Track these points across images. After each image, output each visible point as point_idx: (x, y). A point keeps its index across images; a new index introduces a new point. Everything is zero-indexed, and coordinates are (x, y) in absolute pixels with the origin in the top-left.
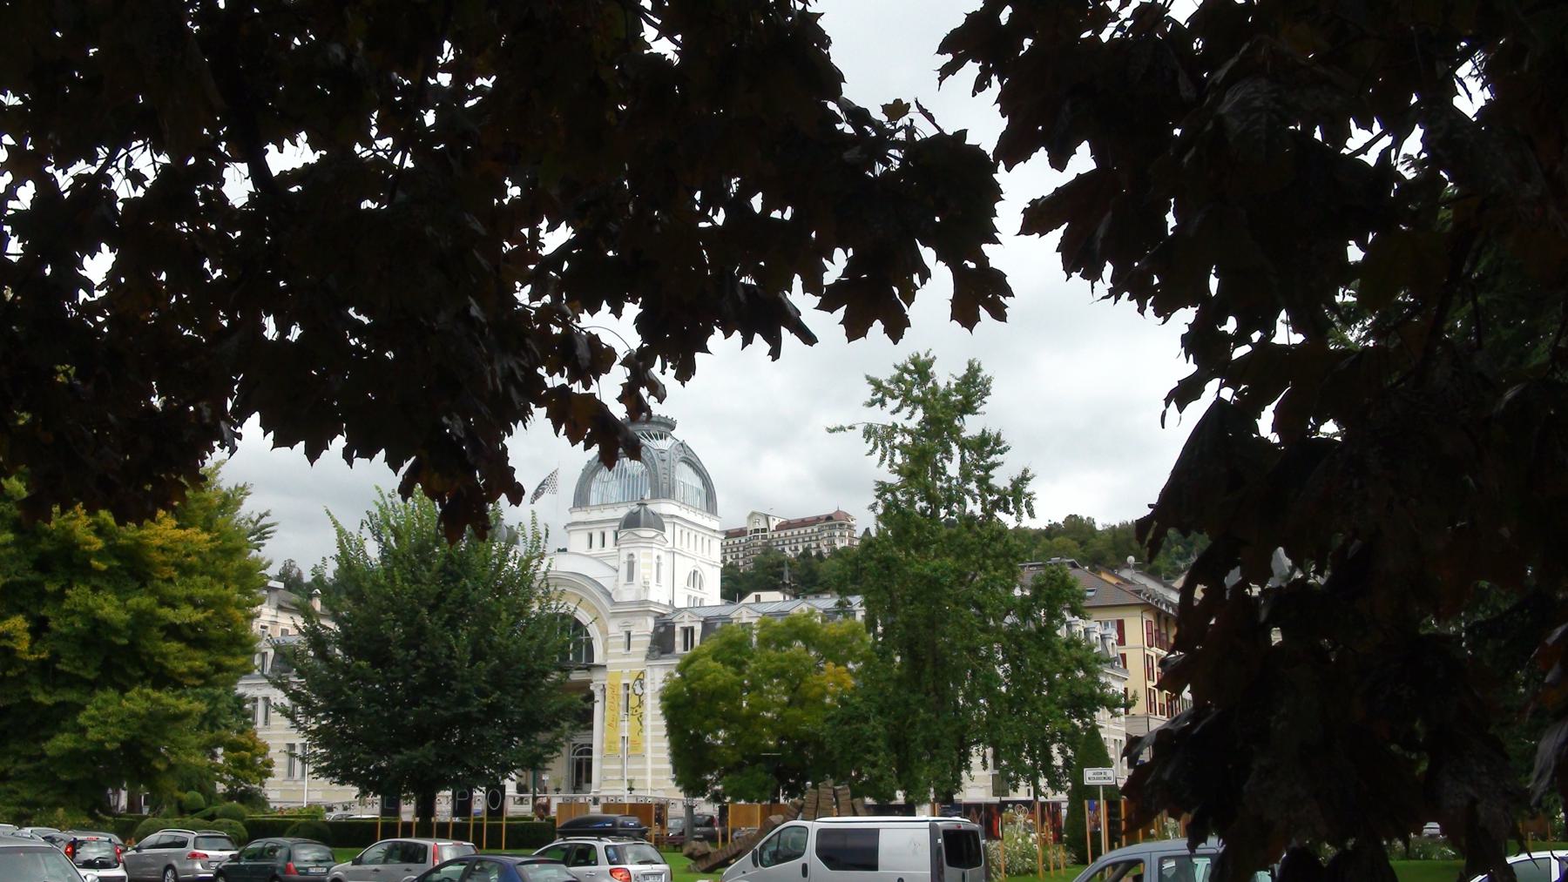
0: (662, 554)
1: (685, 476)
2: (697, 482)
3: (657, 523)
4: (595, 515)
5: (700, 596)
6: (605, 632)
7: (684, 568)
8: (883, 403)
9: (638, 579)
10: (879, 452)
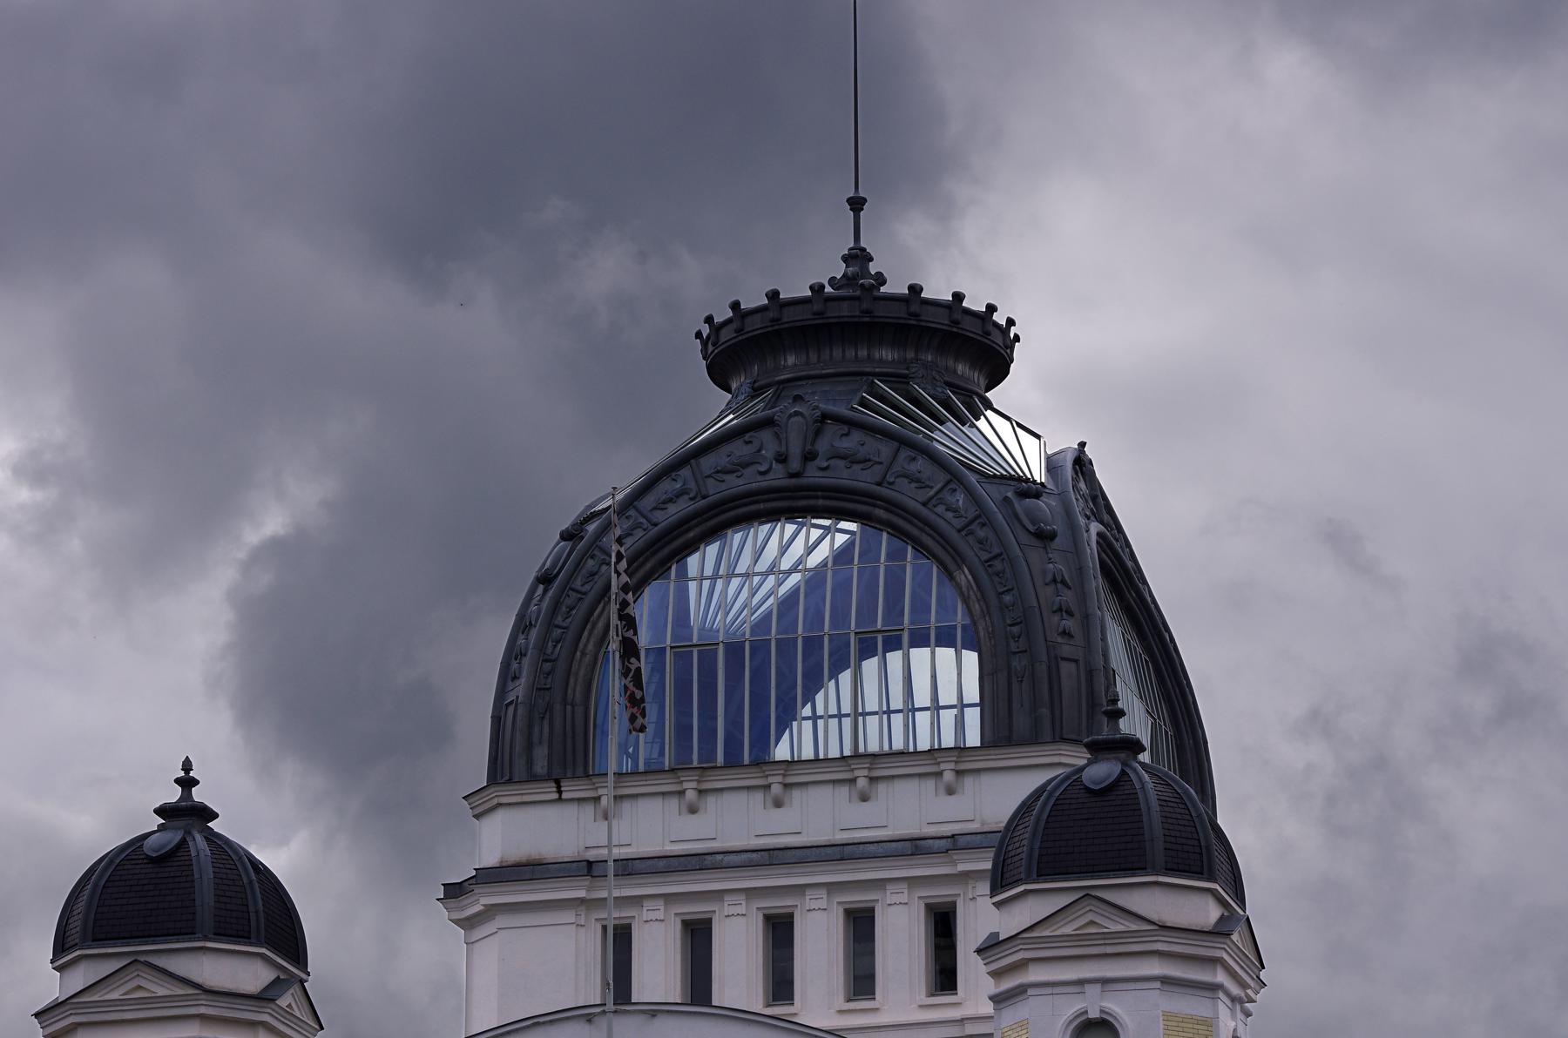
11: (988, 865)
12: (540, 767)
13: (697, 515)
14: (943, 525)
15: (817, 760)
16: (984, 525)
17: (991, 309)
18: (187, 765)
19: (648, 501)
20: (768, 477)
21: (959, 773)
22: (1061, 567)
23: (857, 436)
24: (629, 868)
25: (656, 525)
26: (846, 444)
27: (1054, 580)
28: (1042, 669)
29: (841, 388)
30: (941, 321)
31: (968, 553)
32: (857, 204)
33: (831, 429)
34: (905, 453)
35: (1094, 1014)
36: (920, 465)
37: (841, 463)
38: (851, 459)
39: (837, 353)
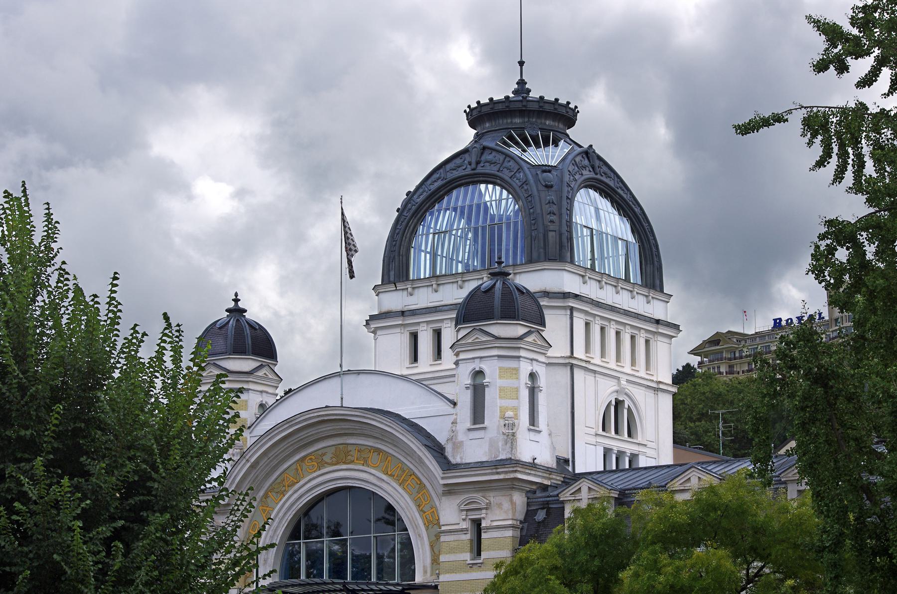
0: (540, 370)
1: (591, 212)
2: (616, 225)
3: (525, 309)
4: (423, 298)
5: (629, 448)
6: (433, 522)
7: (593, 396)
8: (842, 68)
9: (492, 418)
10: (834, 161)
11: (455, 316)
12: (392, 279)
13: (443, 186)
14: (514, 184)
15: (425, 278)
17: (568, 103)
18: (236, 295)
19: (429, 182)
21: (414, 288)
23: (494, 153)
24: (414, 313)
26: (490, 157)
28: (541, 236)
30: (535, 106)
31: (521, 195)
32: (521, 63)
33: (487, 152)
34: (508, 159)
35: (477, 369)
36: (512, 163)
37: (487, 164)
38: (491, 163)
39: (501, 121)
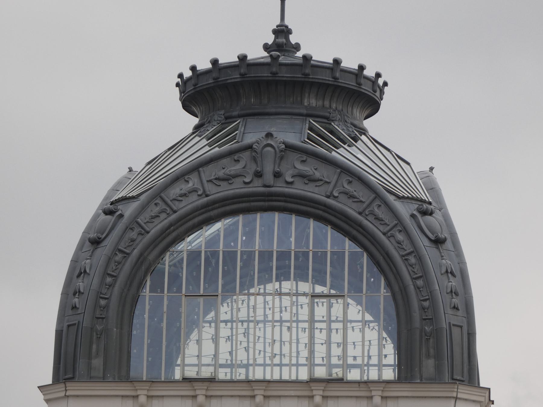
16: (400, 231)
20: (251, 185)
22: (446, 262)
23: (356, 183)
25: (175, 212)
27: (447, 272)
29: (285, 122)
36: (355, 189)
